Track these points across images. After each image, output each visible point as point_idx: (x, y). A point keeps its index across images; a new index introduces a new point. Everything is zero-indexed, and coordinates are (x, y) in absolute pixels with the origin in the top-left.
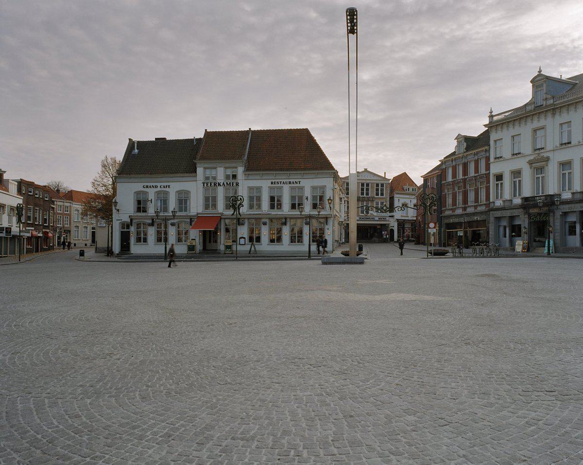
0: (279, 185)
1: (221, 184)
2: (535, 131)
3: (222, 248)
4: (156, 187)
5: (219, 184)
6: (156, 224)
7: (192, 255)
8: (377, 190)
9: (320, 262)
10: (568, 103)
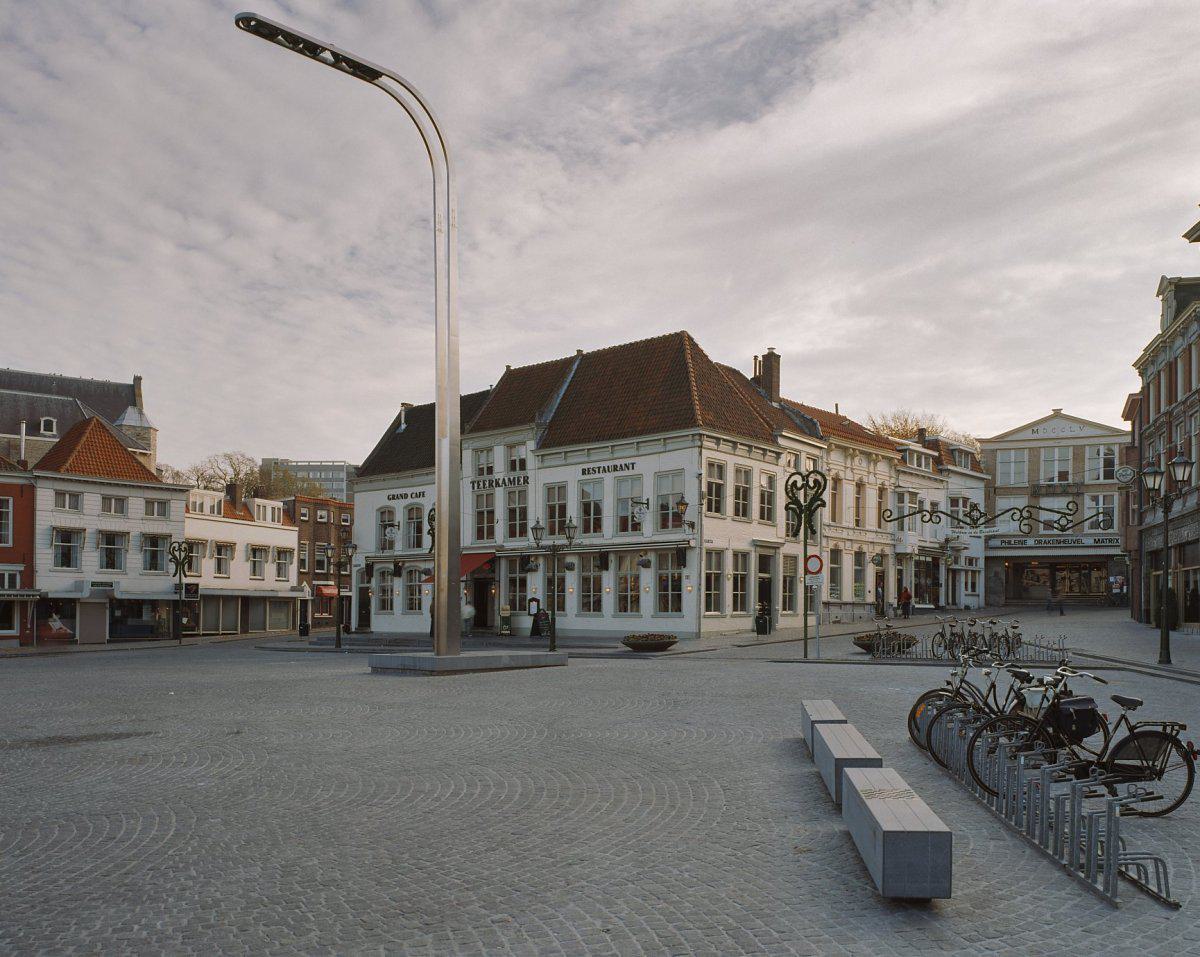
0: (597, 475)
1: (500, 482)
5: (498, 484)
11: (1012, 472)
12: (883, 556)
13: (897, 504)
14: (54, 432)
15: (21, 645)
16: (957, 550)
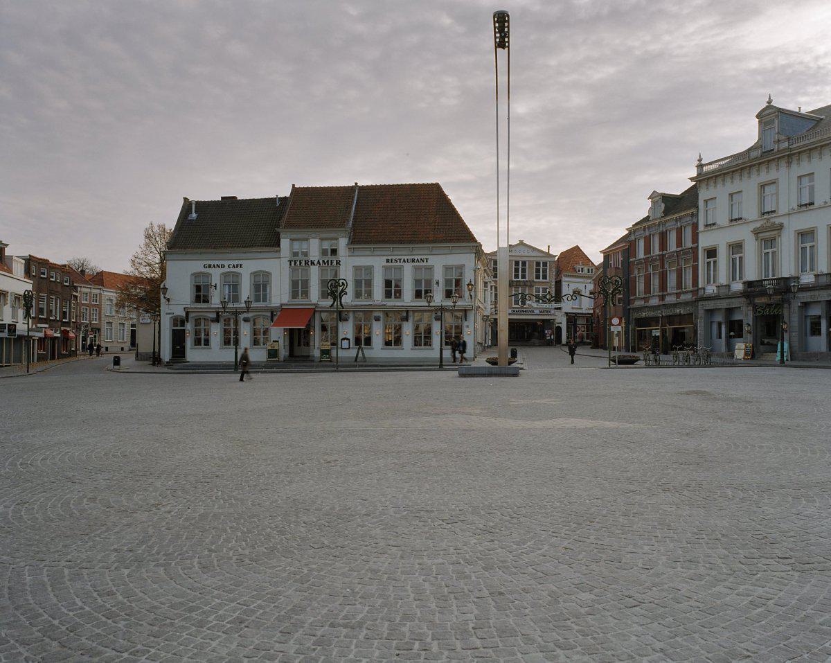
0: (398, 264)
1: (316, 263)
2: (763, 186)
3: (316, 353)
4: (223, 266)
5: (312, 263)
6: (222, 320)
7: (274, 364)
8: (538, 271)
9: (456, 373)
10: (809, 147)
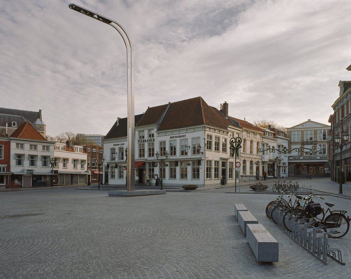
0: (175, 139)
1: (146, 141)
5: (146, 141)
11: (296, 138)
12: (258, 162)
13: (262, 147)
14: (16, 126)
15: (6, 188)
16: (280, 160)
